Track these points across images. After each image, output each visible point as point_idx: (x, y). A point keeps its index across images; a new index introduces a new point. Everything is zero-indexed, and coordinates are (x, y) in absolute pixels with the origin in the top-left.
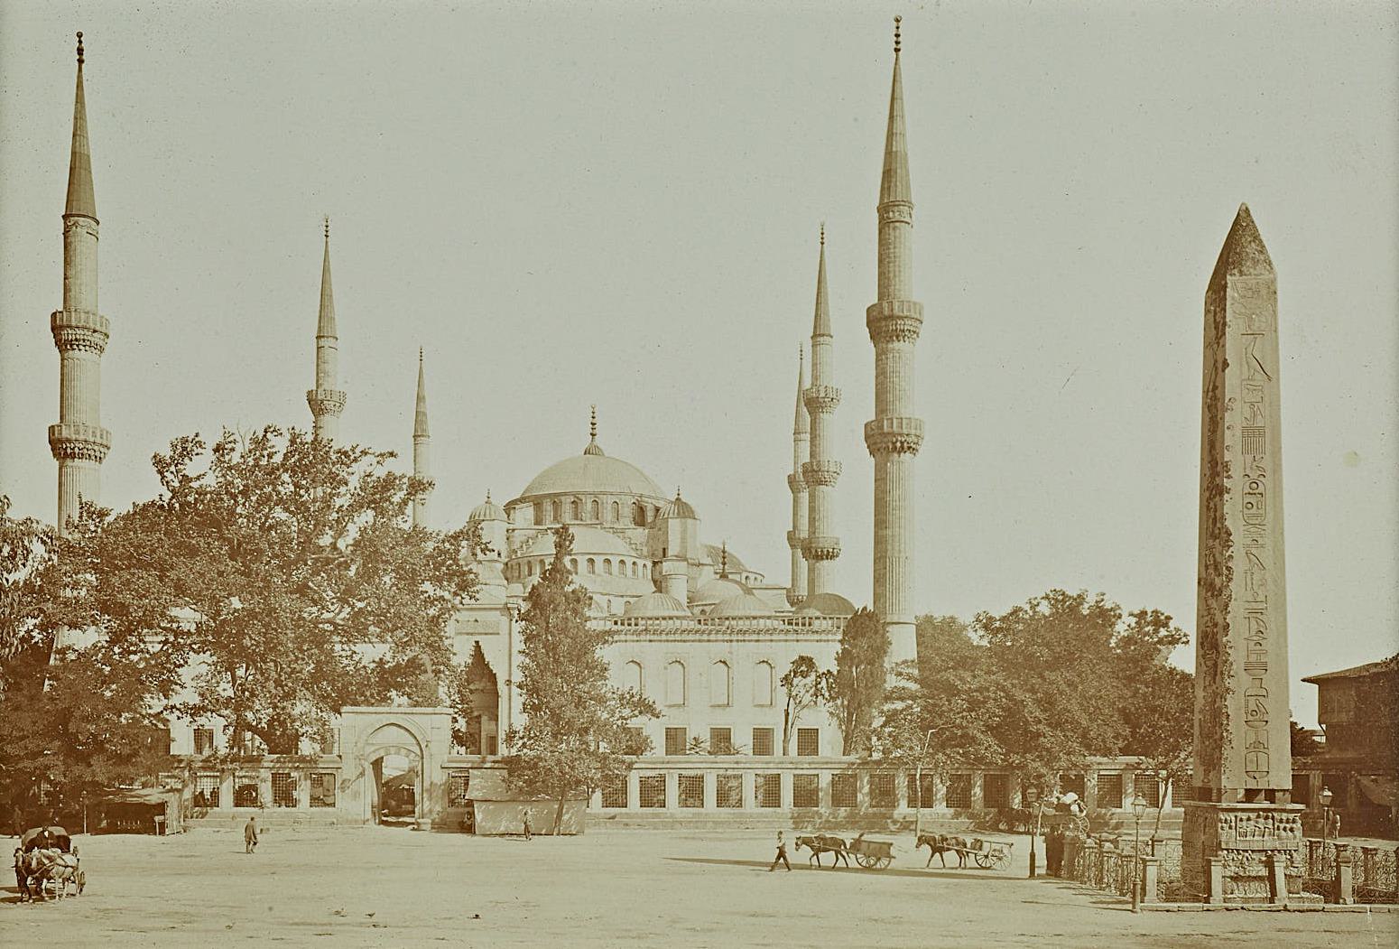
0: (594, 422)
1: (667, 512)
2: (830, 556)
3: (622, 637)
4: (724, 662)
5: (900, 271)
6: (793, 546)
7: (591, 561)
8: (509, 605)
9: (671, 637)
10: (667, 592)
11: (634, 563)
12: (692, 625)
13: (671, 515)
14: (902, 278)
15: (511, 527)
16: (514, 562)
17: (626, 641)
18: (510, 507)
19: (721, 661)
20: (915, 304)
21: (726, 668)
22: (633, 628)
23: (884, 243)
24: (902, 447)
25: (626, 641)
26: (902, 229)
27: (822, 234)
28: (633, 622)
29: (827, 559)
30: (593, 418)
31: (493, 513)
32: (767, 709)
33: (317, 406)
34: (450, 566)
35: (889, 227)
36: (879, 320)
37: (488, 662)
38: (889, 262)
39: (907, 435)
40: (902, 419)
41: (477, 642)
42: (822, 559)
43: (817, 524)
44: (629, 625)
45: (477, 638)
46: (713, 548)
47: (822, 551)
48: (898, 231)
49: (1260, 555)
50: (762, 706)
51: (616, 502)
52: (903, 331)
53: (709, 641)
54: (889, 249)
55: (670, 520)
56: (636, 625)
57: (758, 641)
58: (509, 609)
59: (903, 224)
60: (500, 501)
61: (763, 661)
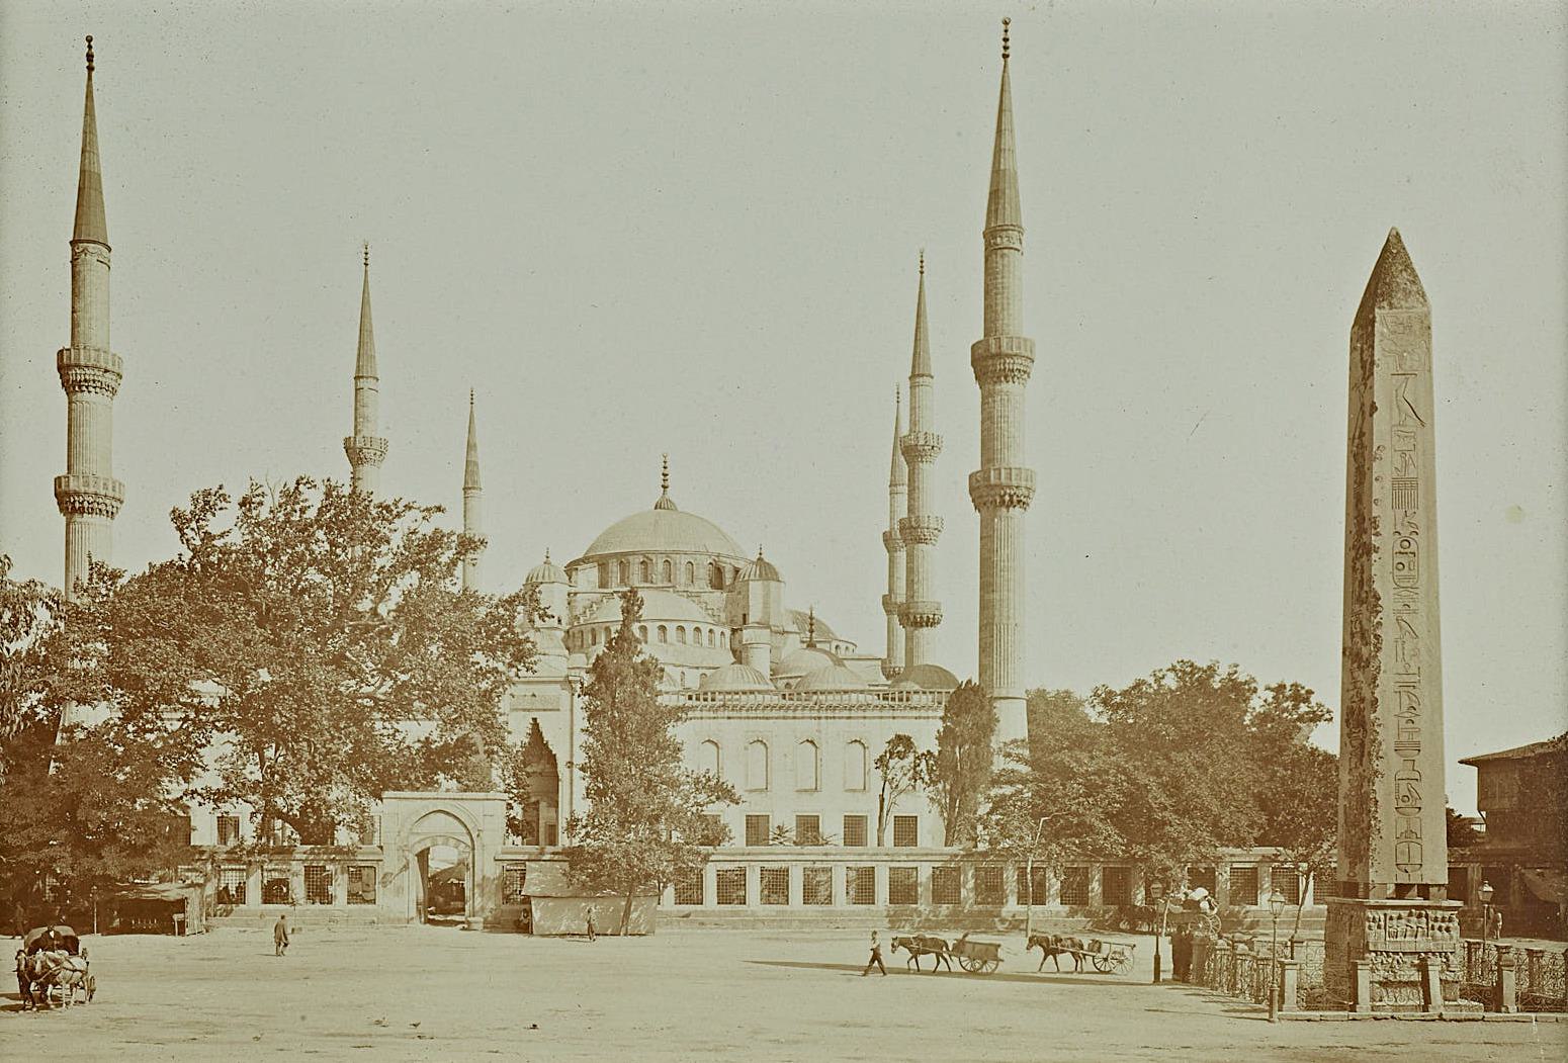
0: (666, 472)
1: (747, 574)
2: (931, 623)
3: (698, 714)
4: (812, 742)
5: (1008, 304)
6: (889, 612)
8: (570, 678)
9: (752, 714)
10: (747, 663)
11: (711, 631)
12: (776, 700)
13: (752, 577)
14: (1011, 312)
15: (573, 590)
16: (576, 630)
17: (702, 718)
18: (571, 568)
19: (808, 741)
20: (1025, 340)
21: (814, 749)
22: (710, 703)
24: (1011, 501)
25: (702, 718)
26: (1011, 257)
28: (709, 696)
29: (927, 626)
30: (665, 468)
31: (552, 575)
32: (860, 794)
33: (355, 455)
34: (504, 634)
35: (996, 254)
37: (547, 742)
38: (996, 294)
39: (1017, 487)
40: (1010, 469)
41: (535, 719)
42: (922, 626)
43: (915, 587)
44: (705, 700)
45: (535, 715)
46: (800, 614)
47: (921, 617)
48: (1006, 259)
50: (854, 791)
51: (690, 562)
52: (1013, 371)
53: (794, 718)
54: (996, 278)
55: (750, 582)
56: (713, 700)
57: (849, 718)
58: (570, 682)
59: (1012, 251)
60: (561, 562)
61: (856, 741)
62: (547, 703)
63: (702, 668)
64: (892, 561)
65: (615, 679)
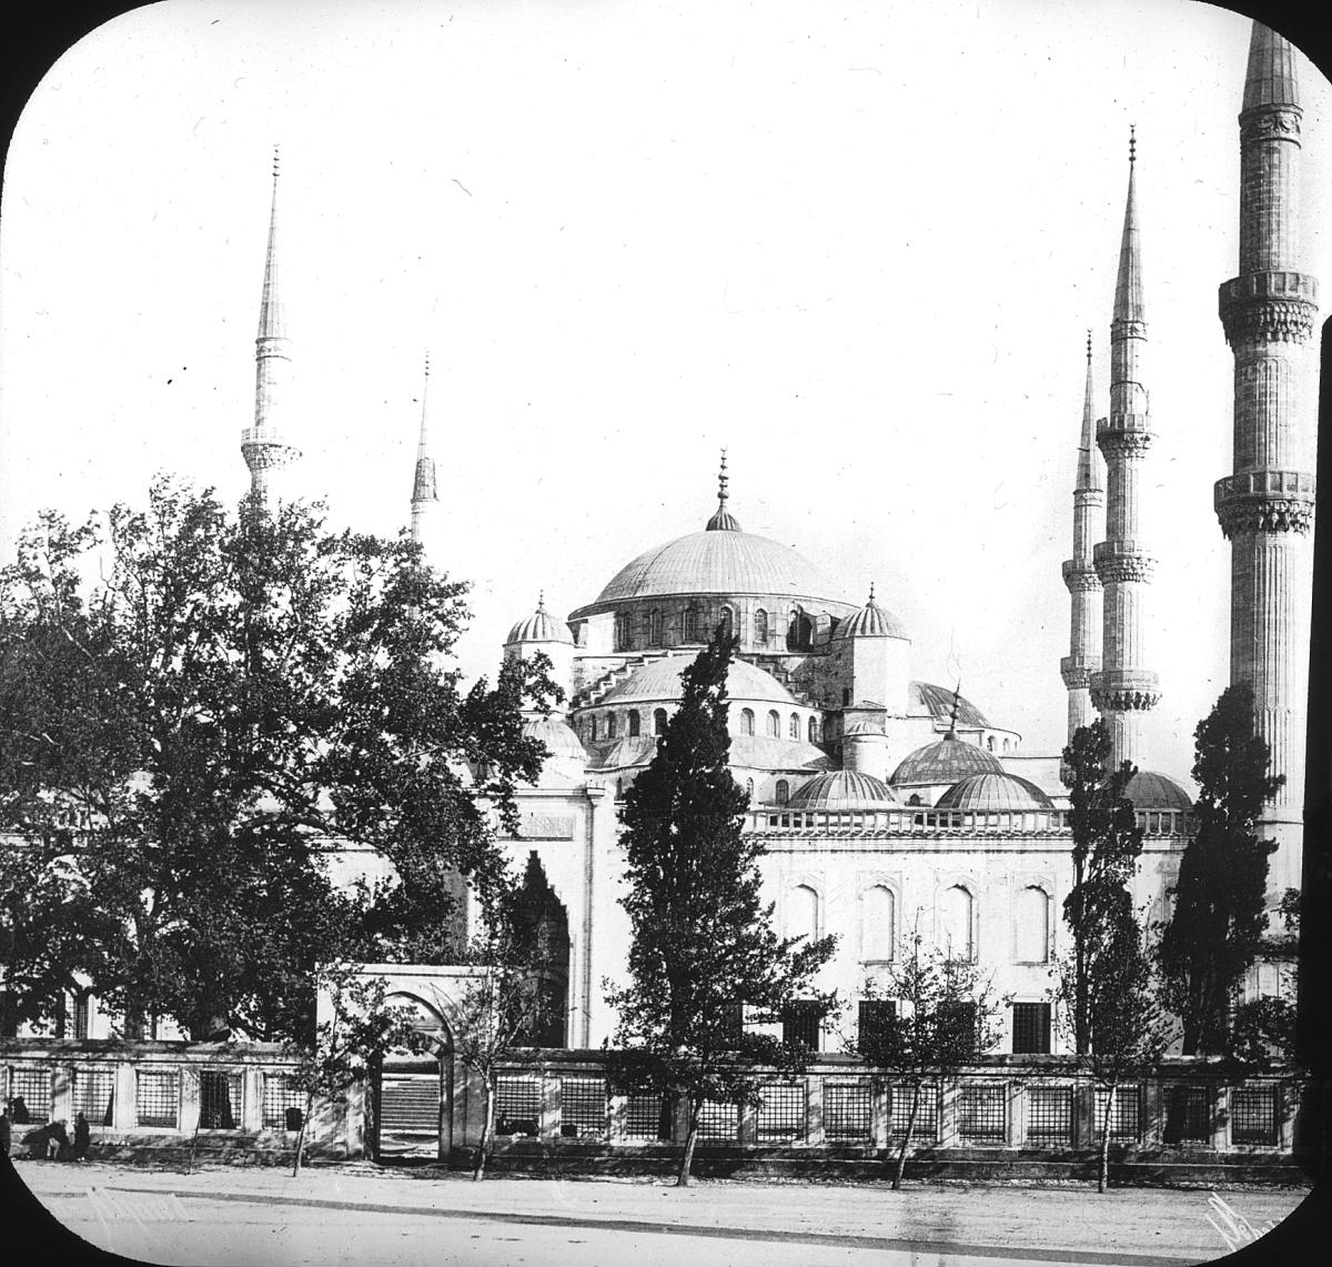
0: (725, 473)
1: (859, 626)
2: (1142, 702)
3: (785, 845)
4: (963, 888)
5: (1278, 223)
6: (1071, 685)
7: (774, 713)
8: (590, 792)
9: (870, 845)
10: (853, 766)
11: (795, 715)
12: (906, 824)
13: (858, 633)
14: (1282, 234)
15: (580, 653)
16: (585, 714)
17: (791, 852)
18: (576, 621)
19: (957, 886)
20: (1305, 277)
21: (967, 898)
22: (804, 829)
23: (1078, 518)
24: (1281, 522)
25: (791, 852)
26: (1283, 150)
27: (1089, 342)
28: (804, 818)
29: (1137, 707)
30: (723, 467)
31: (548, 630)
32: (1038, 968)
33: (254, 455)
34: (495, 727)
35: (1260, 148)
36: (1074, 573)
37: (553, 887)
38: (1260, 208)
39: (1289, 501)
40: (1281, 474)
41: (534, 854)
42: (1128, 707)
43: (1118, 647)
44: (797, 824)
45: (534, 846)
46: (930, 687)
47: (1127, 695)
48: (1276, 155)
49: (763, 691)
50: (1029, 965)
51: (761, 610)
52: (1285, 323)
53: (937, 851)
54: (1260, 185)
55: (856, 640)
56: (809, 824)
57: (1022, 852)
58: (589, 797)
59: (1284, 143)
60: (560, 611)
61: (1032, 887)
62: (570, 835)
63: (781, 771)
64: (1078, 609)
65: (684, 815)
